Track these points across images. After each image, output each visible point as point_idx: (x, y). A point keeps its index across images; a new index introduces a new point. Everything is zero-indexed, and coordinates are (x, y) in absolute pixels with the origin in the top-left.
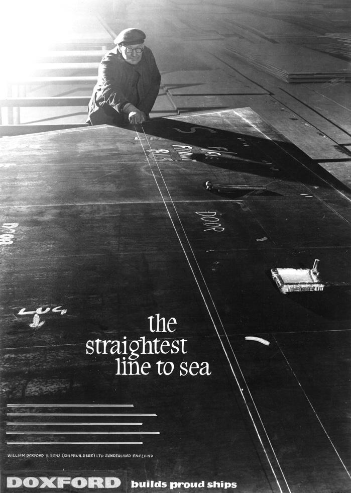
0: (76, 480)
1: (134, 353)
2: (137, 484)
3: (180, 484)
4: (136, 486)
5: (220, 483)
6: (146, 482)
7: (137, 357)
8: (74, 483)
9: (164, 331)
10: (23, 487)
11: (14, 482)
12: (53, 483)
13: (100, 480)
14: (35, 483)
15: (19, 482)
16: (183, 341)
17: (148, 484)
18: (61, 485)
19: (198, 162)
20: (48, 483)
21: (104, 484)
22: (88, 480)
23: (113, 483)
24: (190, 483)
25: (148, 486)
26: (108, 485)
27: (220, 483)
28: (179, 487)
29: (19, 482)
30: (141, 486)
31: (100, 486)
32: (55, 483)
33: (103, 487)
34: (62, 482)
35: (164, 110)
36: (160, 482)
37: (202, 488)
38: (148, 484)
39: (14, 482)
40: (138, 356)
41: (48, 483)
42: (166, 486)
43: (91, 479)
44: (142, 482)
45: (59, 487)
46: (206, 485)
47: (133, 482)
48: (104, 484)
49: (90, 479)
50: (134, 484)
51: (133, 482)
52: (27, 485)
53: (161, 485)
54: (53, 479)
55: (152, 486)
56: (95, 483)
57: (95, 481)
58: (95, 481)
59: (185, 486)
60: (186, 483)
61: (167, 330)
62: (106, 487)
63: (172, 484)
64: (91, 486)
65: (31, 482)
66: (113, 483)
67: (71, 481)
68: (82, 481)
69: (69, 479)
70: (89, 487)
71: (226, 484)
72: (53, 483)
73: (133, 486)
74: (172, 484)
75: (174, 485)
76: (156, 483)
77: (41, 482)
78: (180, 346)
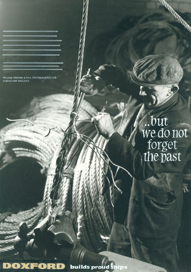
0: (41, 264)
1: (164, 148)
2: (73, 267)
3: (96, 267)
4: (73, 268)
5: (118, 266)
6: (79, 266)
7: (166, 150)
8: (40, 266)
9: (177, 137)
10: (11, 269)
11: (7, 266)
12: (22, 266)
13: (54, 265)
14: (19, 266)
15: (9, 266)
16: (179, 154)
17: (80, 267)
18: (32, 267)
19: (119, 91)
20: (25, 266)
21: (56, 267)
22: (47, 265)
23: (61, 266)
24: (124, 266)
25: (80, 268)
26: (58, 268)
27: (118, 266)
28: (96, 268)
29: (9, 266)
30: (75, 268)
31: (54, 268)
32: (29, 266)
33: (55, 269)
34: (33, 266)
35: (50, 132)
36: (86, 266)
37: (77, 269)
38: (80, 267)
39: (7, 266)
40: (167, 150)
41: (25, 266)
42: (89, 268)
43: (49, 264)
44: (76, 266)
45: (31, 268)
46: (91, 268)
47: (71, 265)
48: (56, 267)
49: (48, 264)
50: (72, 267)
51: (71, 265)
52: (44, 264)
53: (87, 268)
54: (28, 264)
55: (82, 268)
56: (51, 267)
57: (51, 265)
58: (51, 265)
59: (99, 268)
60: (99, 267)
61: (178, 136)
62: (57, 269)
63: (92, 267)
64: (49, 268)
65: (16, 266)
66: (61, 266)
67: (38, 265)
68: (41, 267)
69: (37, 264)
70: (48, 269)
71: (121, 267)
72: (22, 266)
73: (71, 268)
74: (92, 267)
75: (93, 267)
76: (84, 267)
77: (22, 266)
78: (177, 156)
